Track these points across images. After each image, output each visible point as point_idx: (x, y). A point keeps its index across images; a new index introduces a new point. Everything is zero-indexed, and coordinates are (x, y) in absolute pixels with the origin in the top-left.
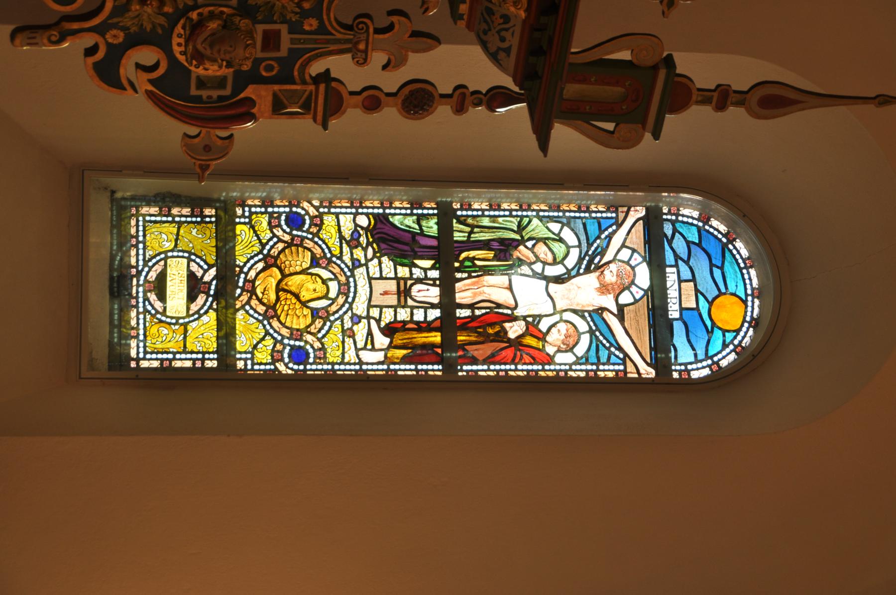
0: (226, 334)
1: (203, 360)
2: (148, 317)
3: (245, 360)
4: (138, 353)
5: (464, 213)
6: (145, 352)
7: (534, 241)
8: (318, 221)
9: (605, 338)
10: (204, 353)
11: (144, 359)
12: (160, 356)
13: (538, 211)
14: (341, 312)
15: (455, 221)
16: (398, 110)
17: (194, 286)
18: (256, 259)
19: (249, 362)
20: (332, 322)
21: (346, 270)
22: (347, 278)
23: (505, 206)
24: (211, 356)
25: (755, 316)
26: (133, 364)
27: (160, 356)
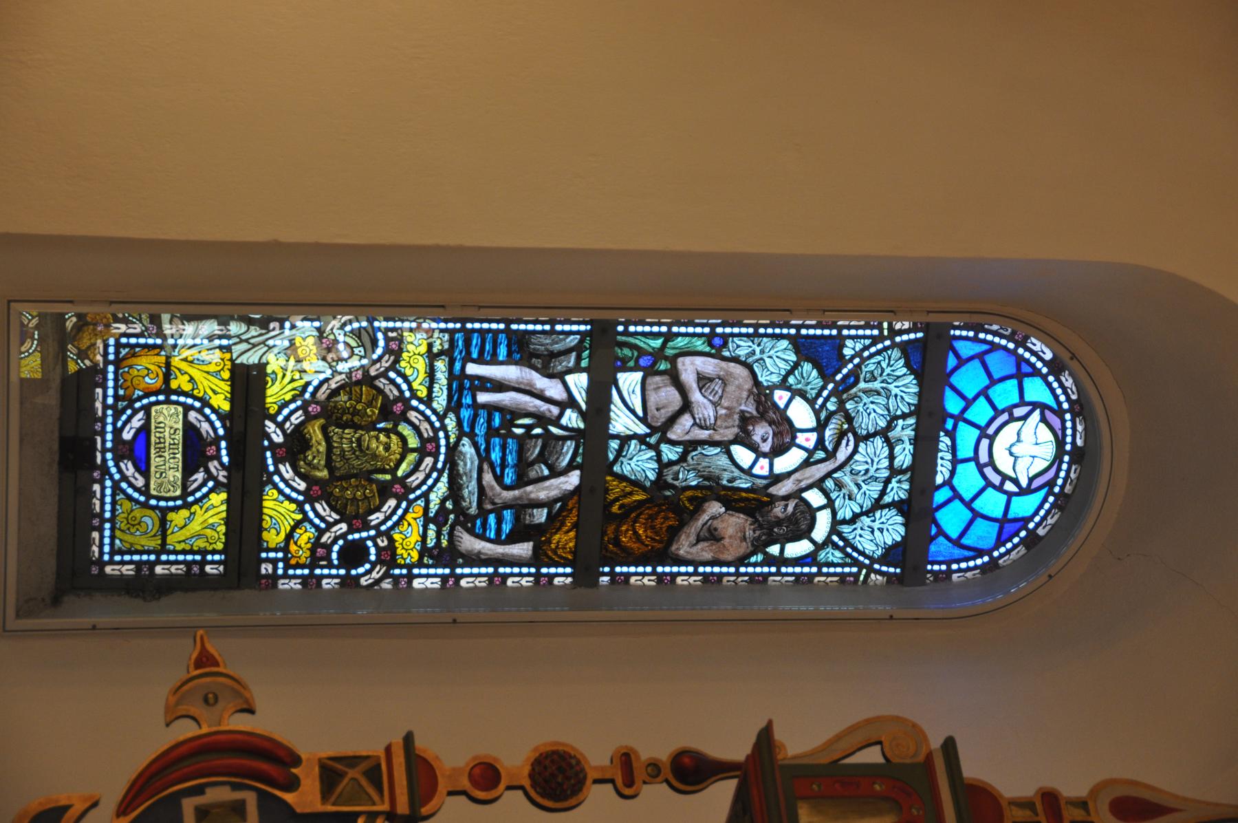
0: (244, 521)
1: (204, 562)
2: (657, 343)
3: (274, 562)
4: (101, 553)
5: (806, 570)
6: (113, 552)
7: (1029, 408)
8: (394, 345)
9: (644, 334)
10: (203, 552)
11: (111, 562)
12: (136, 558)
13: (124, 478)
14: (424, 488)
15: (942, 434)
16: (1001, 796)
17: (195, 450)
18: (292, 406)
19: (281, 565)
20: (410, 503)
21: (433, 418)
22: (435, 431)
23: (295, 585)
24: (217, 557)
25: (1079, 442)
26: (95, 570)
27: (136, 558)
